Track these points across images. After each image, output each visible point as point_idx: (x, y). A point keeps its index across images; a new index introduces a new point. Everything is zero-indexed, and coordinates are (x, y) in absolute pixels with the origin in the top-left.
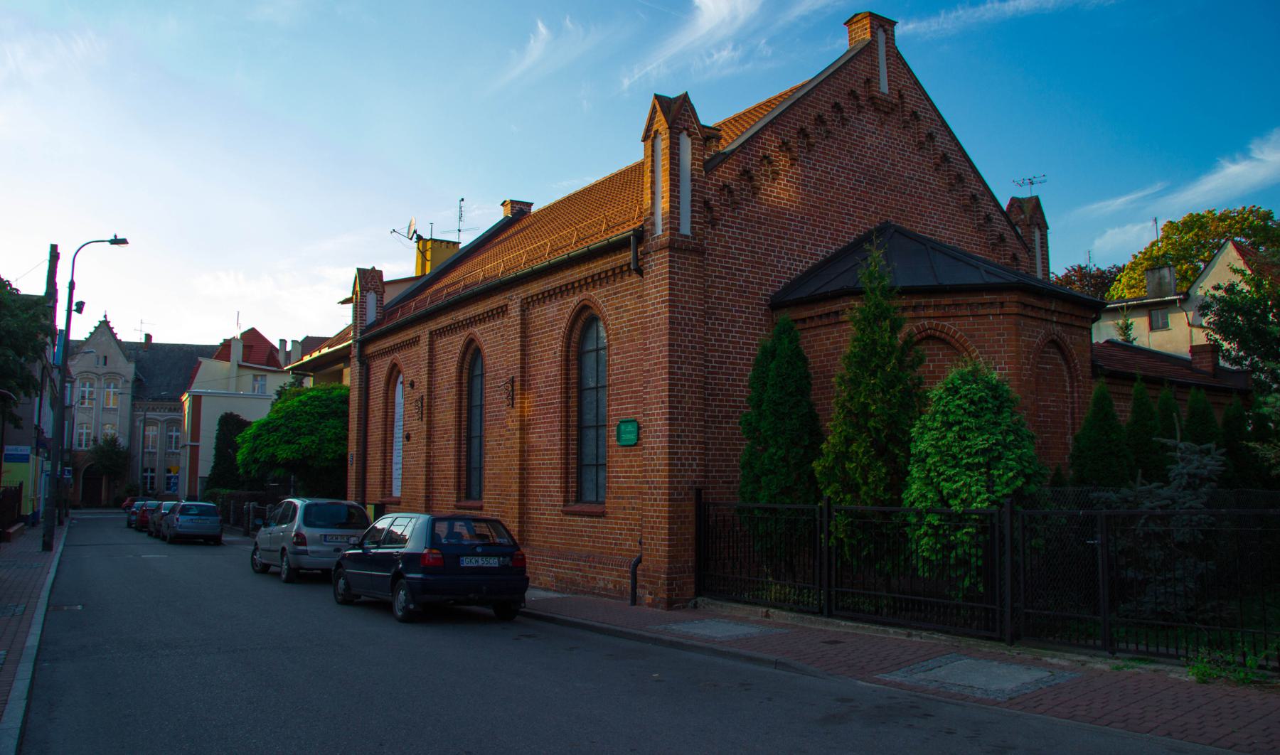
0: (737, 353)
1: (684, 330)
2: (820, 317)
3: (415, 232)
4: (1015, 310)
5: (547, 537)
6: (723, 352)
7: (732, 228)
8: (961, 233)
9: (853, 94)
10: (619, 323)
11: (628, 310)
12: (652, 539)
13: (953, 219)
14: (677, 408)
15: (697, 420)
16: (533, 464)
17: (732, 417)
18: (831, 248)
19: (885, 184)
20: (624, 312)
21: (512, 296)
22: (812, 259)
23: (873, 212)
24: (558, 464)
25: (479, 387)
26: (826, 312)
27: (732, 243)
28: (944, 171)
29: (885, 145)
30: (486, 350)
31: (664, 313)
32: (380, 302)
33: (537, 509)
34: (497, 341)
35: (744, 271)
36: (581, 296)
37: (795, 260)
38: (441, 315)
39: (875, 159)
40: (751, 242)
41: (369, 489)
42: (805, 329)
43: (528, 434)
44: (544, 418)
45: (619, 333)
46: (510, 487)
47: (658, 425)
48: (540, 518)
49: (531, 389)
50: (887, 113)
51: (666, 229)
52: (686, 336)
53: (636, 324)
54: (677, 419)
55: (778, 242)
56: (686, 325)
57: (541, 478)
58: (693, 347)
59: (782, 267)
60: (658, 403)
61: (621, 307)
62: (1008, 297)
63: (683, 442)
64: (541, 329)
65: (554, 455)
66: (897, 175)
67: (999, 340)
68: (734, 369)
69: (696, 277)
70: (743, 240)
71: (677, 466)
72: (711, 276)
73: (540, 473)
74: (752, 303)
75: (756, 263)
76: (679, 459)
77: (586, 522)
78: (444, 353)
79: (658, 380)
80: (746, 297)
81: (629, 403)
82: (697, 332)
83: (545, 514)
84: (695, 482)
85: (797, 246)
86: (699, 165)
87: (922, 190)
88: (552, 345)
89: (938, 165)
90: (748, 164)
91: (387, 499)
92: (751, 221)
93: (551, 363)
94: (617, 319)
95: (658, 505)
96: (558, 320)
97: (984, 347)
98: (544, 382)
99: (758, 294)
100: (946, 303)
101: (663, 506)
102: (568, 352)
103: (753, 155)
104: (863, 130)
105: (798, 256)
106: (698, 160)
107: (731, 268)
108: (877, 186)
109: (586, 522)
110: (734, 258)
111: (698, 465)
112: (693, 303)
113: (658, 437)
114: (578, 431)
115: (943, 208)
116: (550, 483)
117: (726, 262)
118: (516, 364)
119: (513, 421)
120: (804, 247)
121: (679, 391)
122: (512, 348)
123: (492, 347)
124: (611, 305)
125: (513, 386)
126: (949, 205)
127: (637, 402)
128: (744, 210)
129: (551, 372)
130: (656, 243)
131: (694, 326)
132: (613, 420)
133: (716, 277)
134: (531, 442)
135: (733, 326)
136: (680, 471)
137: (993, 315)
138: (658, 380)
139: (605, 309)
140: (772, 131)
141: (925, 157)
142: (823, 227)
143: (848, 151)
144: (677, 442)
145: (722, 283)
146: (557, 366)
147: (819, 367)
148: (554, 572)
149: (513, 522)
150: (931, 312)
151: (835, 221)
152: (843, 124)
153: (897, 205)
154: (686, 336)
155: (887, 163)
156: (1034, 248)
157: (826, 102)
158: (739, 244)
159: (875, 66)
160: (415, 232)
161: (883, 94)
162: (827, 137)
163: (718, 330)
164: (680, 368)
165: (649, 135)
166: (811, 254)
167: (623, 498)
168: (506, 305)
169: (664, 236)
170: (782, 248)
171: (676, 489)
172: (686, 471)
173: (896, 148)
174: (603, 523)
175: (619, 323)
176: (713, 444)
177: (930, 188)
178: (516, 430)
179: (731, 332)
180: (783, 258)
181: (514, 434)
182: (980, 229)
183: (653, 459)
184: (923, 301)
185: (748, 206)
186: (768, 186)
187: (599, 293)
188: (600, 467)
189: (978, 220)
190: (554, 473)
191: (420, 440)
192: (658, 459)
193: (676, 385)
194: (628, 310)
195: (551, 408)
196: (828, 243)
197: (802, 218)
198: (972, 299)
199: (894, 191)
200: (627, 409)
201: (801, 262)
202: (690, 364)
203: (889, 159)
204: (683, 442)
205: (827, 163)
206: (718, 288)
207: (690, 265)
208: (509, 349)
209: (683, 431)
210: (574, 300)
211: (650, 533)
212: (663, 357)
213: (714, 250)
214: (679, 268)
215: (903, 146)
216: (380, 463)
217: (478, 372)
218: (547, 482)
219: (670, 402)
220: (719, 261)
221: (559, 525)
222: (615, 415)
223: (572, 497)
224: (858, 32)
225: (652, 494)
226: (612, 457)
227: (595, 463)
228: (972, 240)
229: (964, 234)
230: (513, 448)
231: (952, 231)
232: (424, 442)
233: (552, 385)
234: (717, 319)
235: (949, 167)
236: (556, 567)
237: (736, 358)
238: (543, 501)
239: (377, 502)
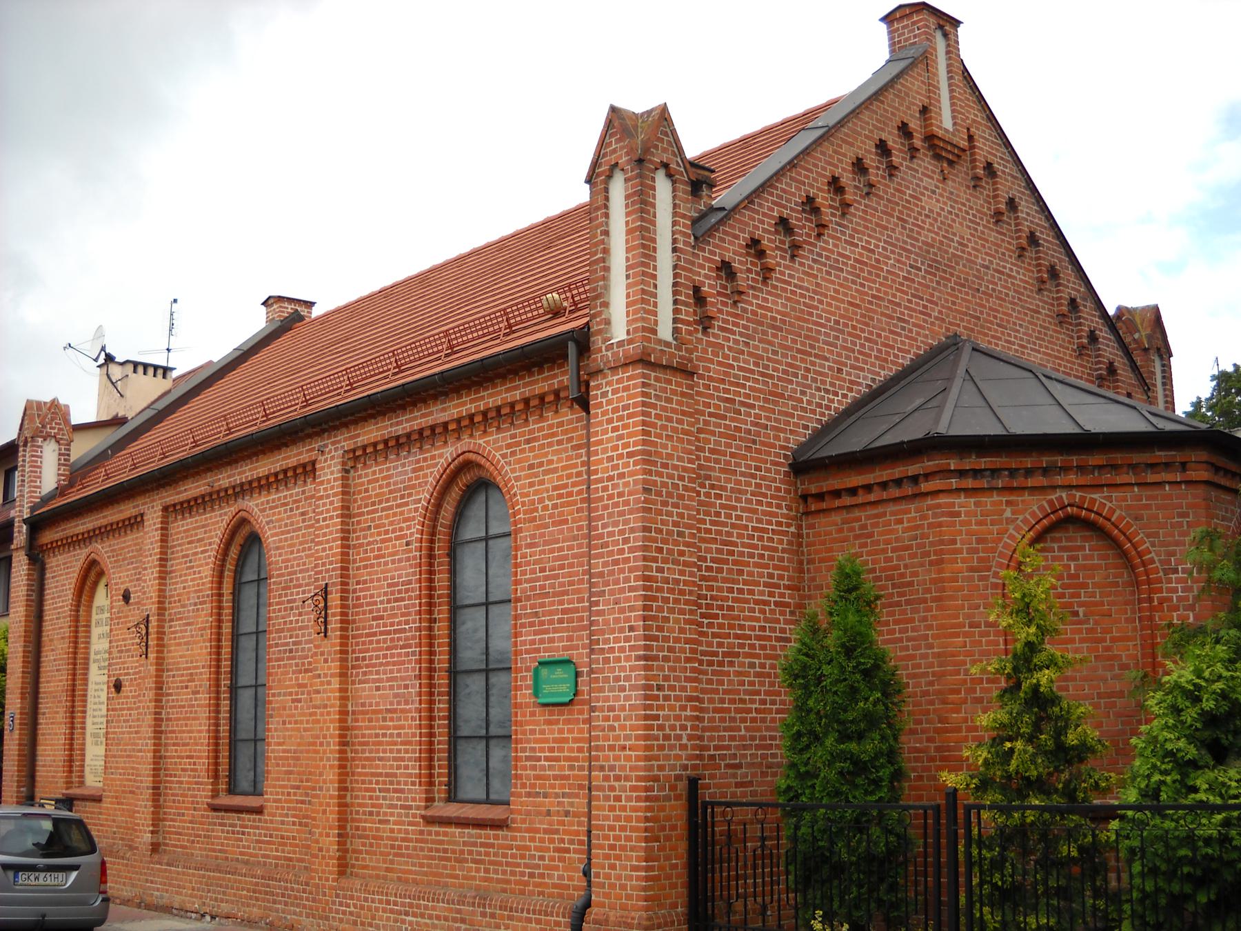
0: (744, 545)
1: (665, 504)
2: (884, 485)
3: (103, 349)
4: (1204, 475)
5: (392, 862)
6: (725, 543)
7: (734, 333)
8: (1057, 357)
9: (904, 130)
10: (536, 492)
11: (555, 470)
12: (613, 867)
13: (1046, 334)
14: (656, 639)
15: (688, 660)
16: (363, 736)
17: (737, 655)
18: (878, 374)
19: (952, 275)
20: (546, 472)
21: (326, 446)
22: (850, 390)
23: (936, 318)
24: (414, 735)
25: (254, 601)
26: (897, 476)
27: (735, 359)
28: (1031, 258)
29: (950, 213)
30: (270, 537)
31: (632, 474)
32: (64, 455)
33: (371, 813)
34: (292, 524)
35: (753, 406)
36: (462, 446)
37: (827, 391)
38: (186, 478)
39: (937, 234)
40: (762, 358)
41: (41, 773)
42: (823, 511)
43: (353, 683)
44: (385, 656)
45: (536, 510)
46: (321, 774)
47: (623, 669)
48: (378, 830)
49: (361, 605)
50: (951, 163)
51: (636, 330)
52: (669, 514)
53: (570, 494)
54: (656, 658)
55: (802, 360)
56: (669, 495)
57: (380, 759)
58: (680, 534)
59: (809, 402)
60: (621, 630)
61: (541, 464)
62: (1195, 455)
63: (667, 698)
64: (380, 502)
65: (406, 719)
66: (968, 260)
67: (1180, 524)
68: (740, 572)
69: (684, 413)
70: (750, 354)
71: (658, 740)
72: (703, 413)
73: (378, 751)
74: (766, 462)
75: (771, 393)
76: (661, 728)
77: (470, 836)
78: (189, 543)
79: (622, 591)
80: (758, 451)
81: (555, 631)
82: (687, 507)
83: (387, 822)
84: (685, 767)
85: (830, 368)
86: (685, 225)
87: (1002, 286)
88: (401, 529)
89: (1023, 249)
90: (757, 228)
91: (75, 791)
92: (761, 324)
93: (400, 561)
94: (531, 485)
95: (623, 809)
96: (413, 487)
97: (1156, 535)
98: (386, 594)
99: (774, 446)
100: (1095, 463)
101: (634, 809)
102: (432, 541)
103: (764, 214)
104: (918, 185)
105: (832, 385)
106: (684, 216)
107: (732, 401)
108: (941, 277)
109: (470, 836)
110: (738, 385)
111: (690, 738)
112: (680, 459)
113: (622, 689)
114: (450, 679)
115: (1032, 317)
116: (399, 767)
117: (727, 391)
118: (331, 563)
119: (326, 661)
120: (840, 371)
121: (660, 609)
122: (325, 535)
123: (283, 533)
124: (519, 461)
125: (326, 600)
126: (1039, 312)
127: (574, 629)
128: (752, 304)
129: (400, 576)
130: (615, 354)
131: (681, 497)
132: (526, 661)
133: (711, 415)
134: (361, 697)
135: (738, 500)
136: (661, 748)
137: (1169, 483)
138: (622, 591)
139: (507, 468)
140: (791, 178)
141: (1005, 235)
142: (867, 339)
143: (899, 218)
144: (657, 698)
145: (719, 426)
146: (411, 566)
147: (883, 570)
148: (411, 923)
149: (328, 835)
150: (1072, 478)
151: (884, 330)
152: (891, 175)
153: (968, 308)
154: (669, 514)
155: (952, 240)
156: (1155, 385)
157: (867, 137)
158: (745, 361)
159: (932, 88)
160: (103, 349)
161: (947, 131)
162: (868, 194)
163: (713, 505)
164: (660, 570)
165: (598, 176)
166: (851, 382)
167: (546, 796)
168: (313, 463)
169: (630, 342)
170: (807, 370)
171: (656, 779)
172: (671, 747)
173: (964, 219)
174: (505, 838)
175: (536, 492)
176: (711, 701)
177: (1013, 284)
178: (332, 675)
179: (735, 508)
180: (810, 387)
181: (329, 683)
182: (1081, 351)
183: (612, 728)
184: (1059, 460)
185: (757, 297)
186: (786, 267)
187: (495, 441)
188: (492, 743)
189: (1079, 338)
190: (407, 751)
191: (140, 696)
192: (623, 728)
193: (655, 599)
194: (555, 470)
195: (399, 639)
196: (873, 365)
197: (837, 322)
198: (1138, 458)
199: (963, 286)
200: (552, 640)
201: (836, 394)
202: (676, 562)
203: (955, 234)
204: (667, 698)
205: (869, 236)
206: (713, 433)
207: (674, 392)
208: (318, 536)
209: (666, 678)
210: (445, 454)
211: (607, 857)
212: (631, 550)
213: (708, 369)
214: (658, 397)
215: (974, 216)
216: (63, 729)
217: (250, 575)
218: (391, 767)
219: (646, 628)
220: (717, 389)
221: (417, 841)
222: (527, 652)
223: (440, 791)
224: (903, 34)
225: (612, 789)
226: (521, 724)
227: (483, 732)
228: (1071, 369)
229: (1061, 359)
230: (325, 706)
231: (1045, 354)
232: (151, 694)
233: (403, 599)
234: (712, 487)
235: (1037, 252)
236: (415, 915)
237: (742, 554)
238: (384, 798)
239: (60, 796)
